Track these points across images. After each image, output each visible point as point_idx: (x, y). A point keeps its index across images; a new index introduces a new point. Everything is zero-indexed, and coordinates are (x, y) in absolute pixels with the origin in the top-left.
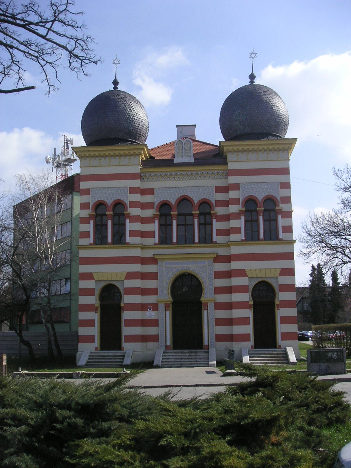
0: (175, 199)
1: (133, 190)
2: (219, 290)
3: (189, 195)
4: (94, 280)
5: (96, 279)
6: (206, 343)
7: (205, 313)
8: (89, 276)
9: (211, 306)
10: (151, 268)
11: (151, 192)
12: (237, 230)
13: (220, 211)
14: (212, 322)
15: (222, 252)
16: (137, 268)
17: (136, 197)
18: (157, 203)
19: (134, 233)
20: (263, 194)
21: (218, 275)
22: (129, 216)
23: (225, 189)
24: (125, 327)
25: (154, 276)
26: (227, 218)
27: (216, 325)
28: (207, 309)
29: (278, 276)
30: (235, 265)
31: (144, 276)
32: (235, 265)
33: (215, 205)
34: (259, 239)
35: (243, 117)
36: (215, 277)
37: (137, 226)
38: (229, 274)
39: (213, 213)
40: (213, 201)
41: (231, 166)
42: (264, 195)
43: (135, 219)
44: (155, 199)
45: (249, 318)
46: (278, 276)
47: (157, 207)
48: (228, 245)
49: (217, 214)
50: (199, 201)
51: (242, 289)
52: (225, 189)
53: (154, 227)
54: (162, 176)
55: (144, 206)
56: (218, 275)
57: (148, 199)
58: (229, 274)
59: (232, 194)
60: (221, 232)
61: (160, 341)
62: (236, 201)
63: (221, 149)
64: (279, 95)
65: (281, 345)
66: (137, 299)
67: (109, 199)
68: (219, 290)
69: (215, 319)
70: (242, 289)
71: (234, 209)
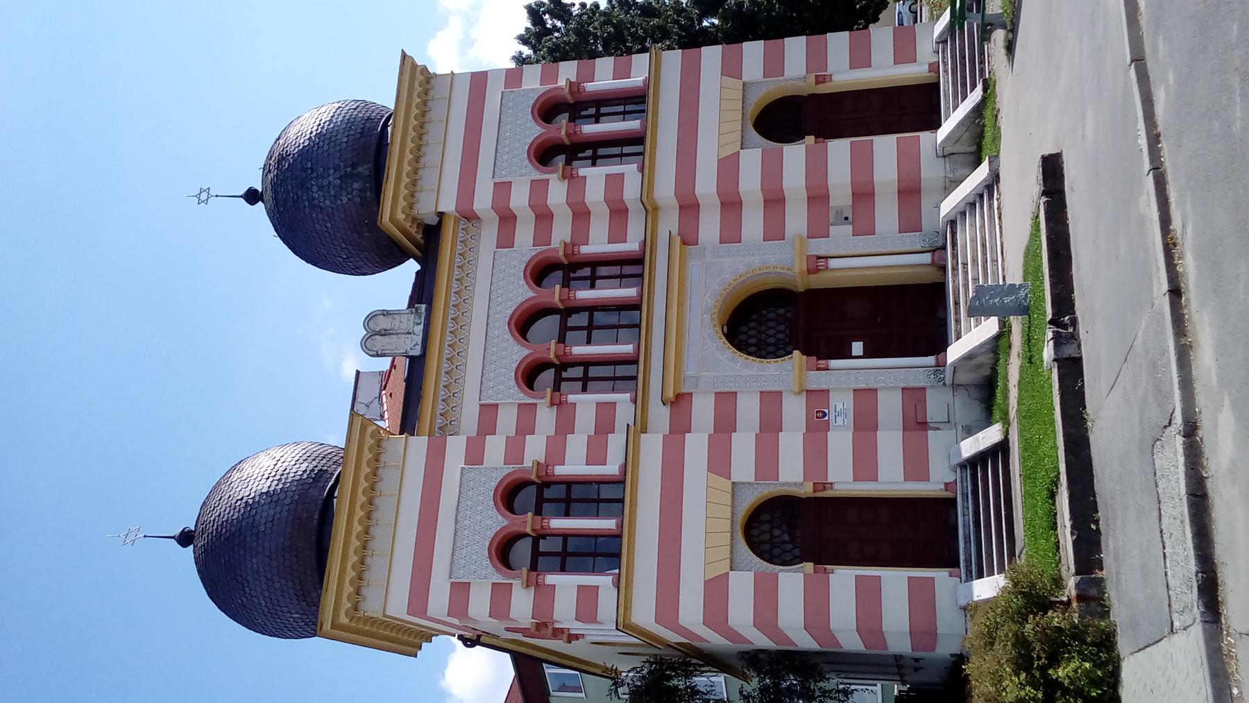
0: (517, 348)
1: (475, 455)
2: (774, 231)
3: (510, 312)
4: (739, 151)
5: (724, 567)
8: (716, 591)
9: (819, 247)
10: (703, 410)
11: (489, 412)
12: (615, 182)
13: (561, 233)
15: (669, 223)
16: (696, 446)
17: (495, 448)
18: (522, 395)
19: (596, 453)
20: (529, 125)
21: (731, 234)
22: (570, 247)
23: (507, 219)
24: (882, 476)
25: (726, 402)
26: (581, 215)
29: (730, 483)
30: (706, 185)
31: (725, 424)
32: (706, 185)
34: (617, 536)
35: (331, 179)
37: (577, 446)
38: (731, 205)
41: (448, 205)
42: (493, 512)
43: (556, 449)
44: (510, 395)
46: (738, 84)
48: (651, 210)
50: (530, 287)
51: (772, 172)
52: (507, 219)
53: (585, 404)
54: (451, 371)
55: (526, 426)
56: (731, 234)
57: (507, 420)
58: (731, 205)
59: (519, 200)
60: (618, 233)
62: (539, 189)
63: (408, 225)
66: (791, 445)
67: (489, 522)
68: (774, 231)
70: (772, 172)
71: (557, 193)
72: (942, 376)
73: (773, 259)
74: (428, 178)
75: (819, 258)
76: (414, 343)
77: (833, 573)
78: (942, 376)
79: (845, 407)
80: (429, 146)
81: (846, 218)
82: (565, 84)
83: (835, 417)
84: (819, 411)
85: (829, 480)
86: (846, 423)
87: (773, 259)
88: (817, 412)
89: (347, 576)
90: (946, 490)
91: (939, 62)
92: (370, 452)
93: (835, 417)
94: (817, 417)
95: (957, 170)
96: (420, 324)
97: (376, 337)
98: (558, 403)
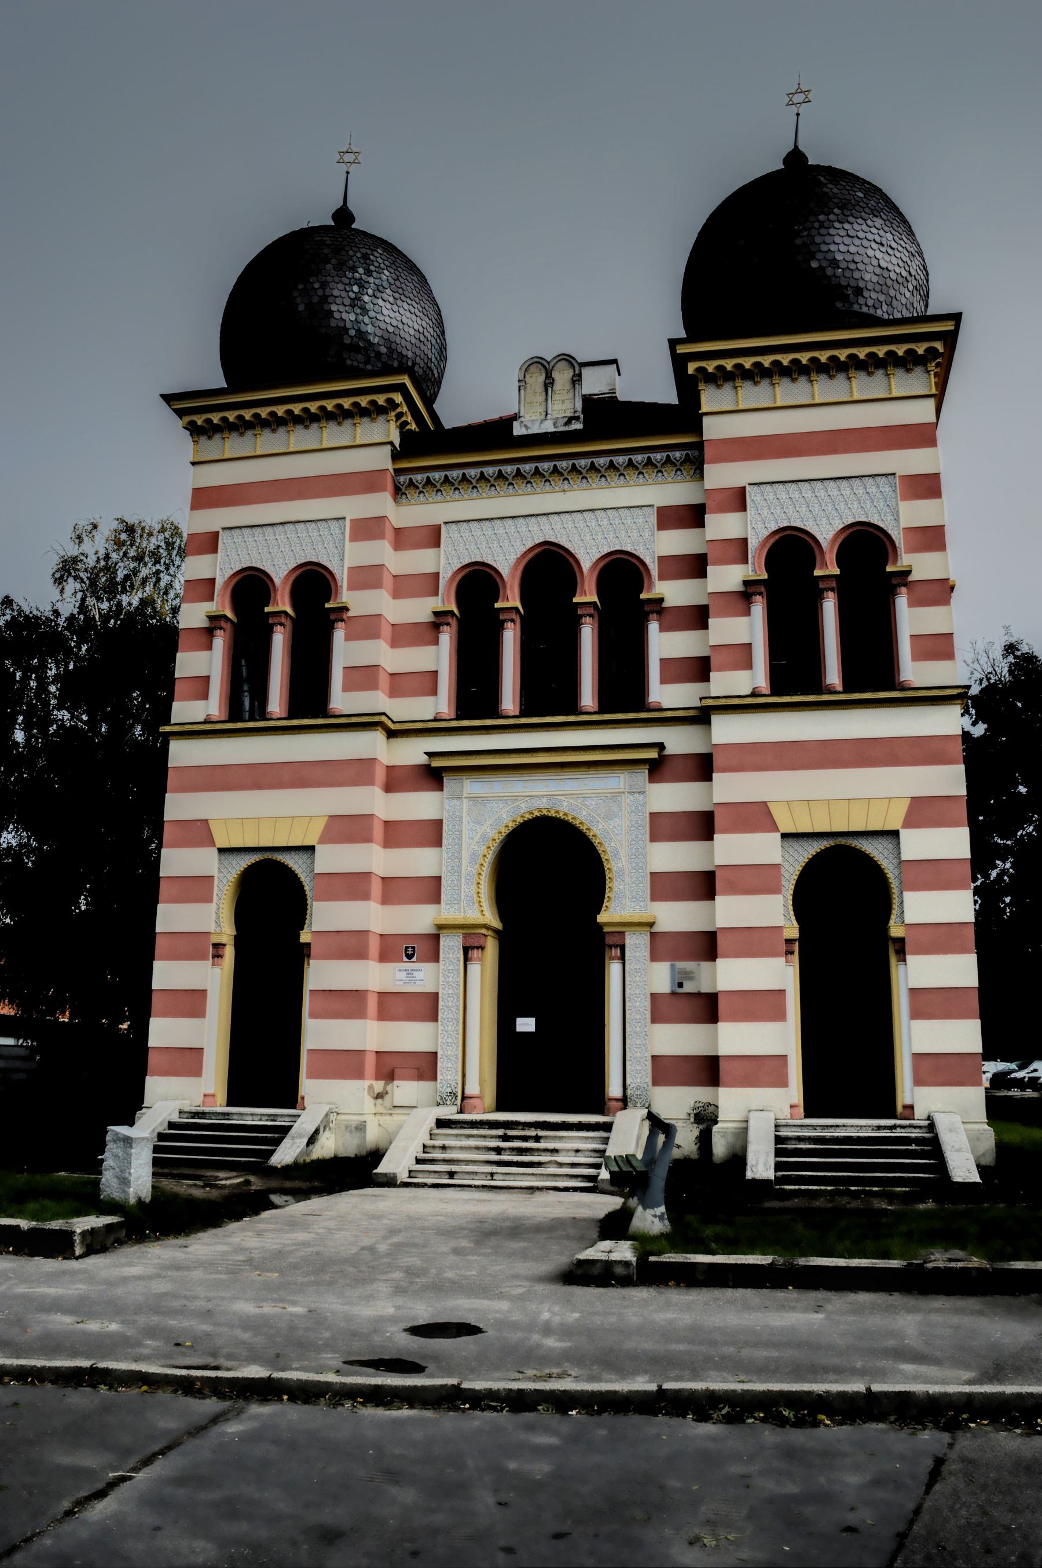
0: (513, 558)
6: (614, 1090)
7: (614, 969)
9: (637, 944)
14: (640, 1007)
18: (449, 574)
27: (654, 1020)
28: (623, 958)
33: (654, 571)
36: (655, 836)
39: (649, 601)
40: (648, 561)
45: (784, 1058)
47: (448, 589)
49: (665, 605)
61: (439, 1077)
62: (739, 549)
64: (919, 237)
65: (911, 1107)
69: (654, 1058)
72: (448, 1102)
73: (622, 887)
74: (750, 394)
75: (623, 948)
76: (529, 425)
77: (787, 962)
78: (448, 1102)
79: (418, 982)
80: (809, 384)
81: (680, 985)
82: (904, 564)
83: (406, 970)
84: (414, 951)
85: (909, 957)
86: (397, 982)
87: (622, 887)
88: (413, 948)
89: (896, 346)
90: (905, 1107)
91: (914, 1120)
92: (925, 351)
93: (406, 970)
94: (407, 948)
95: (722, 1136)
96: (555, 427)
97: (544, 375)
98: (440, 618)
